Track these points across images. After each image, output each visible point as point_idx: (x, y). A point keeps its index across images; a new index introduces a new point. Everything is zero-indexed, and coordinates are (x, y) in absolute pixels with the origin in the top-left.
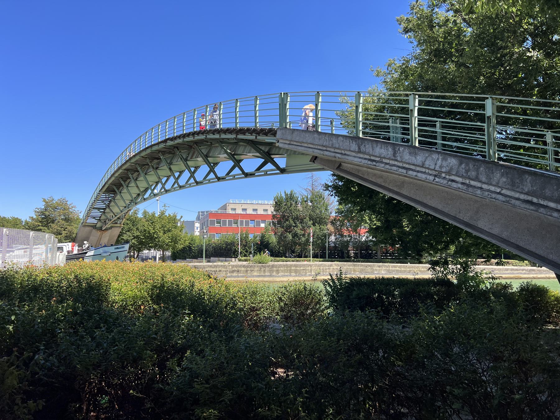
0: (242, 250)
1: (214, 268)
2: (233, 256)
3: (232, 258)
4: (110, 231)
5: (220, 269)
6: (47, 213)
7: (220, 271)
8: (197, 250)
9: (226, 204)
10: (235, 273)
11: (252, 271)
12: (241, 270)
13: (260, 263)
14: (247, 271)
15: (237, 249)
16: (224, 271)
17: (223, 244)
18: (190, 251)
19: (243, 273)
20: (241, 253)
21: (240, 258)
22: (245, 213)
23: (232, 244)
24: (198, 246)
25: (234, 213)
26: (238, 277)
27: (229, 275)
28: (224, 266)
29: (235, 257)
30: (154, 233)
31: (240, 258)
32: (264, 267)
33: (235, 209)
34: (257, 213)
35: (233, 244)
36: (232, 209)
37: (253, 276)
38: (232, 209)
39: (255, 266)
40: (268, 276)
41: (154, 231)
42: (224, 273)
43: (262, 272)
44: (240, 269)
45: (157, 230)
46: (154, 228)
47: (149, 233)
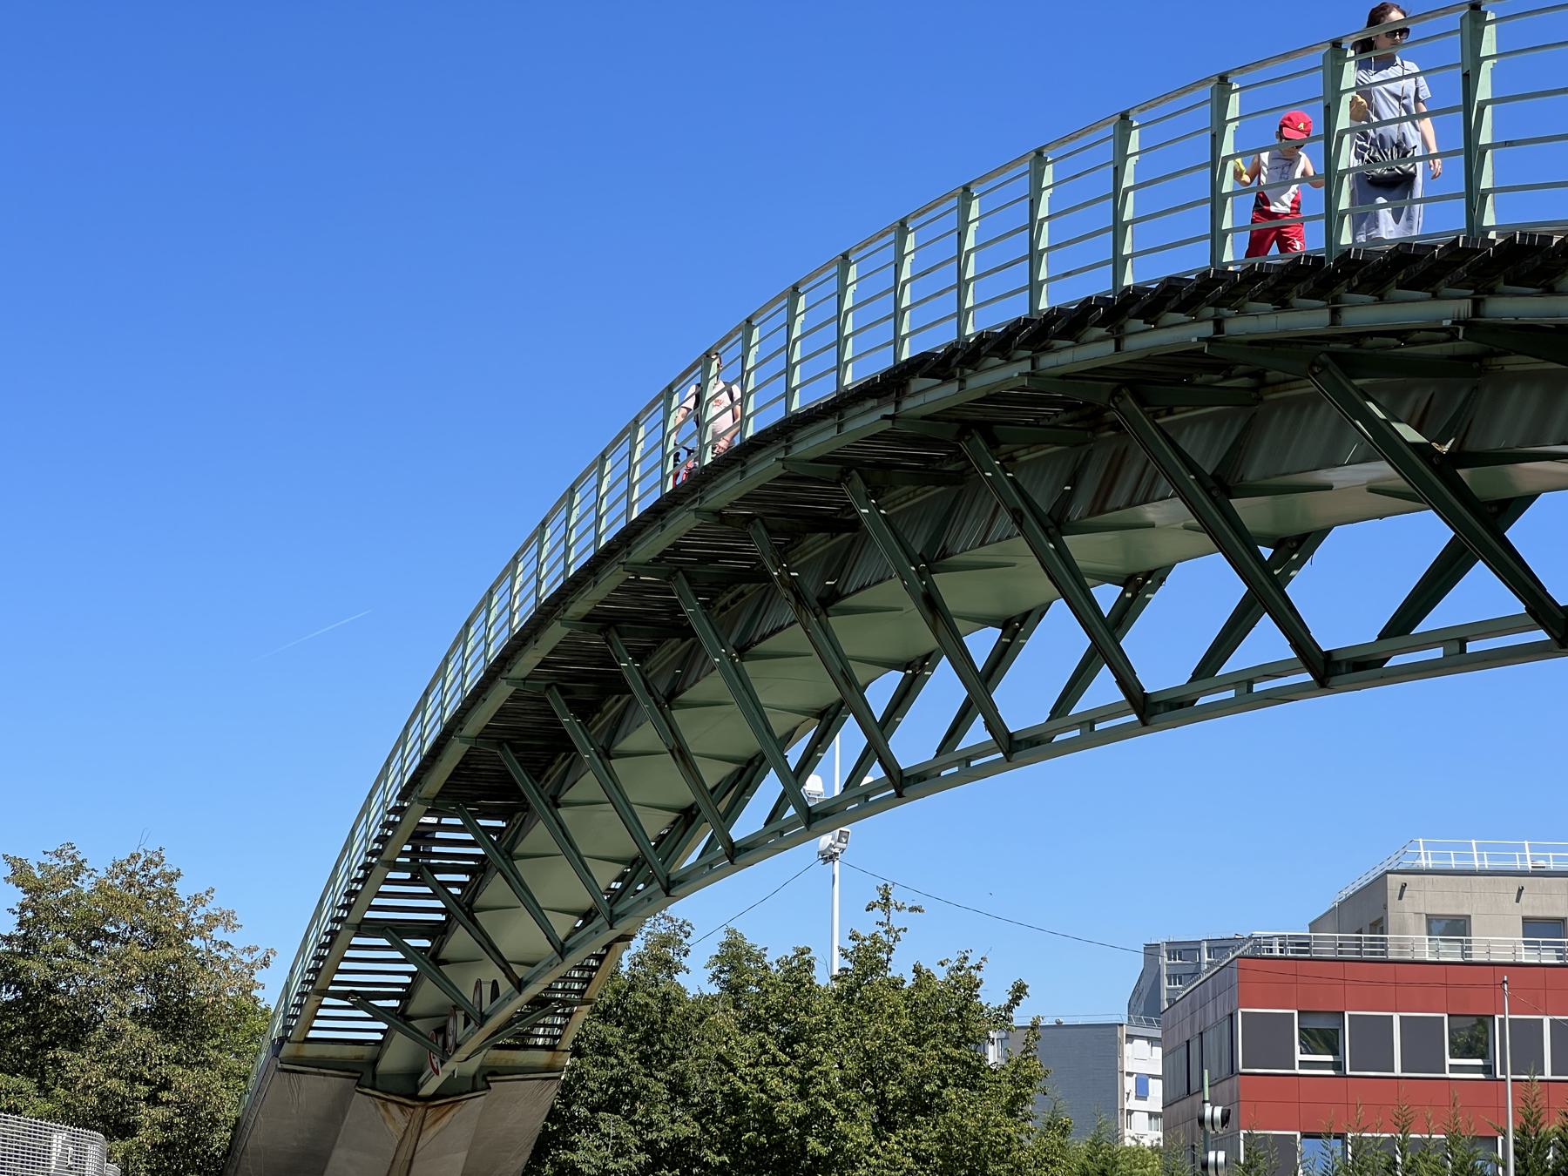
4: (474, 1105)
25: (1451, 953)
30: (803, 1123)
41: (801, 1109)
45: (829, 1095)
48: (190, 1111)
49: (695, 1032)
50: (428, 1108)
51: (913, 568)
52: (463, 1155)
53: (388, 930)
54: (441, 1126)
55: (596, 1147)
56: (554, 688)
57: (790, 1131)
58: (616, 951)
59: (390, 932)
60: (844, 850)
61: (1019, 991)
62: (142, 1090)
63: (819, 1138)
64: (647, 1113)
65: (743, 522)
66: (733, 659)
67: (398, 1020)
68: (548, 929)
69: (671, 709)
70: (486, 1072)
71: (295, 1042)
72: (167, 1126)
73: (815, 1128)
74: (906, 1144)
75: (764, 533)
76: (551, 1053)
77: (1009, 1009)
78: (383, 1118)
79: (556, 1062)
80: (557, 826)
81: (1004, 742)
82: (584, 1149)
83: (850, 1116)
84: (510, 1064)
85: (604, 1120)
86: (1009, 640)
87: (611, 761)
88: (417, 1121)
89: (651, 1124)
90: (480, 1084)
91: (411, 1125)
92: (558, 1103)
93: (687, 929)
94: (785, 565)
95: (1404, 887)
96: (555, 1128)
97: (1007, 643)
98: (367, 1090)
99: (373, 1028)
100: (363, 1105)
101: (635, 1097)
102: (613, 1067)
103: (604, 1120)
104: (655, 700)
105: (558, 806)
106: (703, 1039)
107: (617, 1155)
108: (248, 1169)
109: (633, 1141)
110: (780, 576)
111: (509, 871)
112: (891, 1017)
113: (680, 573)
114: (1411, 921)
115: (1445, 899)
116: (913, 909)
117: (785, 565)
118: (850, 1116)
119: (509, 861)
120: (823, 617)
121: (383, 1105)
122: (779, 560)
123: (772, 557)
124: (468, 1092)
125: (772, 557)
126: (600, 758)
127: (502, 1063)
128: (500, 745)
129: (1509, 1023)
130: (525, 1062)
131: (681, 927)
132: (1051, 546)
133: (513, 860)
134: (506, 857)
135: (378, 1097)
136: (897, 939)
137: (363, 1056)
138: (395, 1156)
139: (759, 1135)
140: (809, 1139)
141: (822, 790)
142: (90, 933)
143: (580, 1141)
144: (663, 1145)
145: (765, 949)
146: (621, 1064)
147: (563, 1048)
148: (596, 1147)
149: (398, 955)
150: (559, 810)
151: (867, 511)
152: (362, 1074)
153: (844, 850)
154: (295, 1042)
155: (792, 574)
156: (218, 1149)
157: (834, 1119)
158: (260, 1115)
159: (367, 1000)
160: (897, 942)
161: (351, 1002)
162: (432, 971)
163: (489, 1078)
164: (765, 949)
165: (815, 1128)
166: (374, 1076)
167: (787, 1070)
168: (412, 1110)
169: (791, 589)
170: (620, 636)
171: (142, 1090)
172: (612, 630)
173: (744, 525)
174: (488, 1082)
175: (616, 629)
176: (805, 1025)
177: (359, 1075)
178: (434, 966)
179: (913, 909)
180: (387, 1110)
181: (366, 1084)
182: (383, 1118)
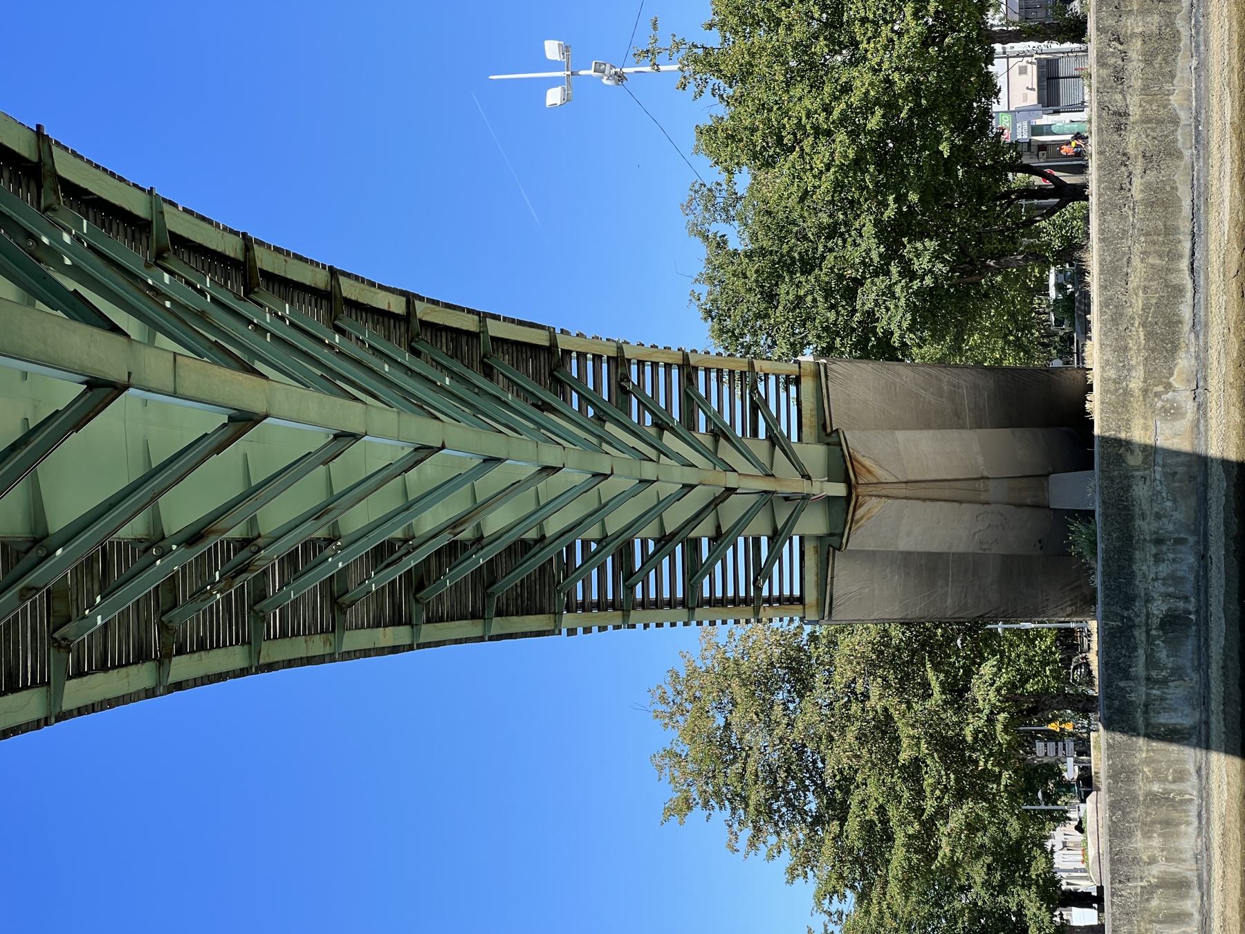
4: (854, 440)
30: (853, 135)
41: (841, 136)
45: (827, 109)
48: (872, 668)
50: (858, 484)
51: (158, 562)
52: (901, 435)
53: (692, 582)
54: (874, 466)
55: (887, 311)
56: (418, 596)
57: (863, 142)
58: (701, 361)
59: (694, 580)
60: (612, 66)
63: (867, 117)
65: (168, 633)
66: (339, 548)
67: (777, 541)
68: (669, 502)
69: (414, 537)
70: (824, 434)
71: (804, 612)
72: (886, 685)
73: (859, 121)
74: (869, 34)
75: (176, 611)
76: (802, 379)
78: (868, 519)
79: (811, 371)
80: (562, 538)
81: (345, 443)
82: (889, 324)
83: (847, 89)
84: (814, 413)
85: (863, 304)
86: (269, 334)
87: (485, 536)
88: (870, 489)
89: (863, 263)
90: (833, 439)
91: (874, 493)
92: (851, 340)
93: (697, 187)
94: (208, 587)
96: (873, 339)
97: (271, 336)
98: (844, 541)
99: (790, 551)
100: (859, 539)
101: (841, 277)
102: (814, 300)
103: (863, 304)
104: (405, 555)
105: (543, 537)
106: (787, 207)
108: (920, 609)
110: (220, 591)
111: (617, 540)
112: (752, 55)
113: (256, 608)
116: (655, 28)
117: (208, 587)
119: (608, 539)
120: (260, 542)
121: (858, 522)
122: (204, 593)
123: (202, 601)
124: (842, 450)
125: (202, 601)
126: (482, 548)
127: (814, 420)
128: (491, 595)
130: (812, 400)
131: (696, 192)
132: (59, 552)
133: (607, 536)
134: (604, 544)
135: (850, 529)
136: (683, 42)
137: (814, 547)
138: (902, 498)
139: (868, 171)
140: (869, 126)
141: (560, 87)
143: (883, 327)
144: (882, 249)
145: (711, 116)
147: (797, 369)
148: (887, 311)
149: (718, 566)
150: (547, 536)
151: (99, 618)
152: (830, 545)
153: (612, 66)
154: (804, 612)
155: (217, 578)
156: (903, 633)
157: (849, 106)
158: (872, 618)
159: (761, 569)
160: (686, 41)
161: (764, 582)
162: (727, 540)
163: (829, 430)
164: (711, 116)
165: (859, 121)
166: (831, 535)
167: (807, 150)
168: (860, 497)
169: (233, 578)
170: (347, 592)
171: (855, 708)
172: (340, 600)
173: (171, 632)
174: (833, 432)
175: (339, 597)
176: (765, 133)
177: (831, 549)
178: (723, 539)
179: (655, 28)
180: (862, 518)
181: (839, 542)
182: (868, 519)
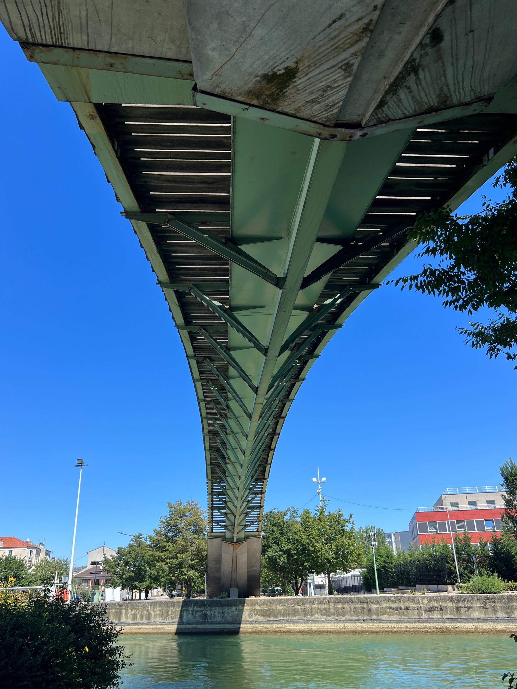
0: (462, 570)
1: (395, 602)
2: (449, 581)
3: (447, 584)
4: (245, 543)
5: (407, 604)
6: (172, 523)
7: (407, 608)
8: (395, 572)
9: (441, 498)
10: (436, 613)
11: (469, 608)
12: (446, 607)
13: (483, 592)
14: (458, 609)
15: (452, 568)
16: (414, 609)
17: (430, 560)
18: (387, 574)
19: (452, 614)
20: (461, 575)
21: (461, 584)
22: (474, 508)
23: (442, 559)
24: (396, 566)
25: (455, 509)
26: (443, 620)
27: (424, 616)
28: (413, 599)
29: (453, 584)
30: (308, 544)
31: (461, 584)
32: (492, 600)
33: (456, 504)
34: (495, 506)
35: (445, 558)
36: (452, 504)
37: (473, 620)
38: (452, 504)
39: (473, 599)
40: (503, 619)
41: (308, 541)
42: (416, 612)
43: (490, 611)
44: (444, 604)
45: (313, 538)
46: (309, 536)
47: (302, 545)
49: (291, 528)
52: (246, 554)
61: (351, 516)
62: (189, 544)
64: (281, 543)
77: (350, 519)
95: (445, 497)
101: (279, 541)
107: (275, 552)
109: (278, 550)
112: (324, 522)
114: (447, 503)
115: (453, 499)
116: (329, 501)
118: (318, 542)
120: (227, 419)
128: (215, 466)
129: (476, 523)
136: (326, 507)
142: (182, 516)
146: (276, 534)
171: (189, 544)
179: (329, 501)
